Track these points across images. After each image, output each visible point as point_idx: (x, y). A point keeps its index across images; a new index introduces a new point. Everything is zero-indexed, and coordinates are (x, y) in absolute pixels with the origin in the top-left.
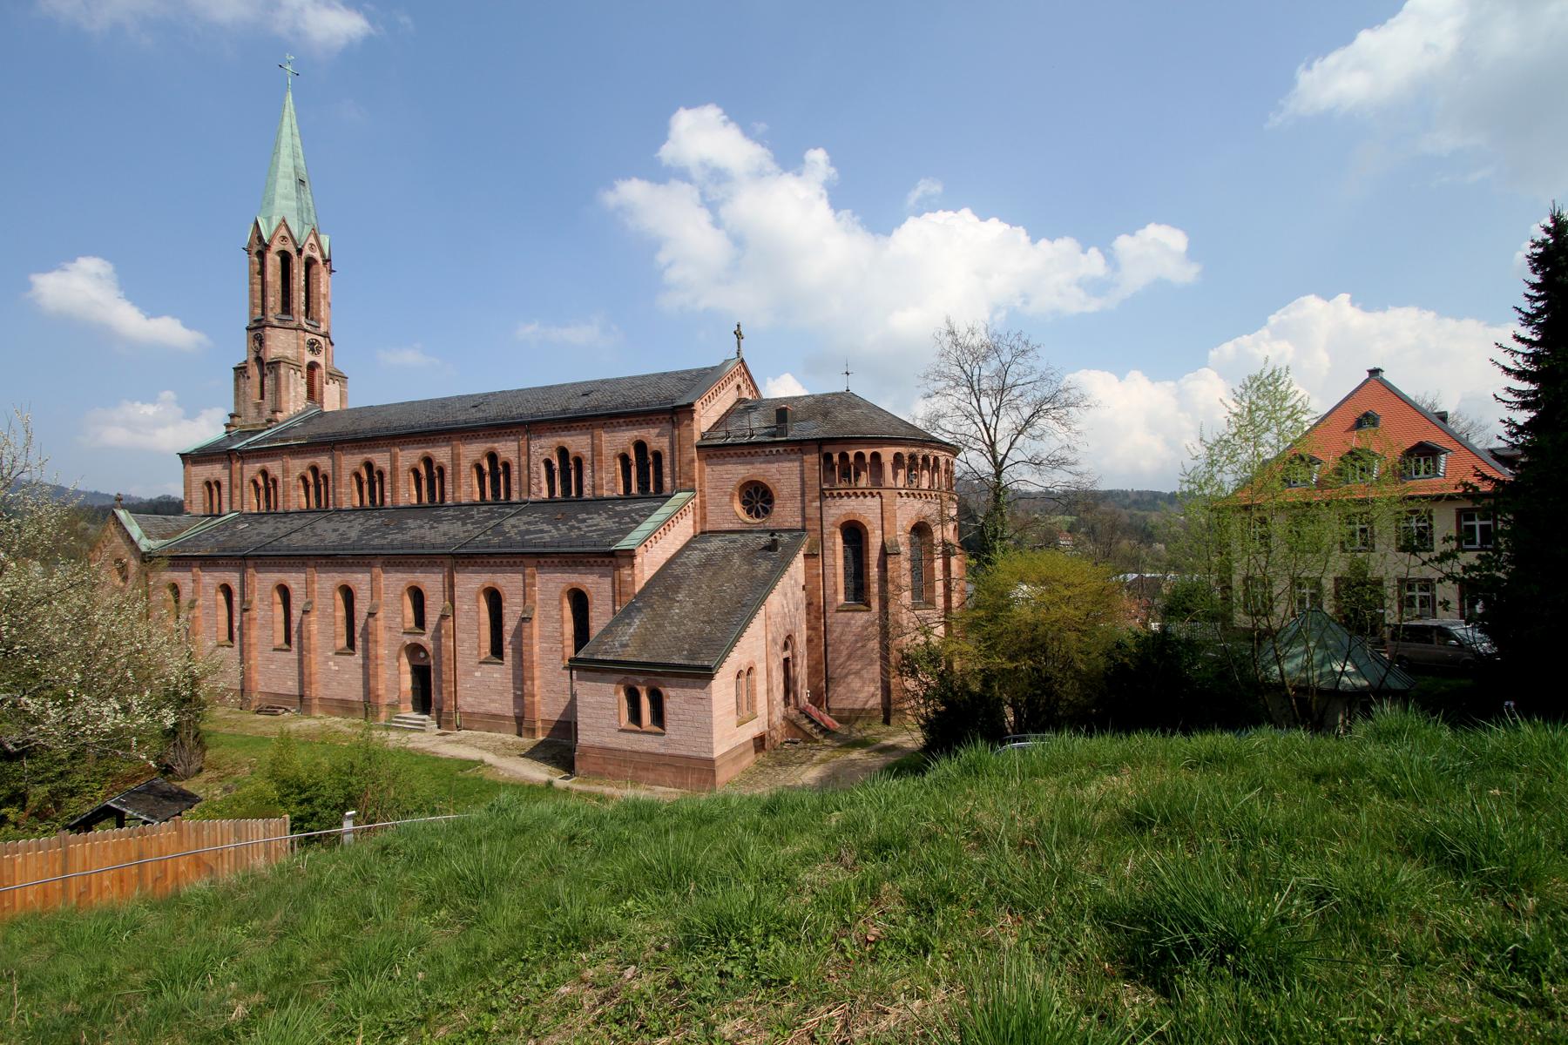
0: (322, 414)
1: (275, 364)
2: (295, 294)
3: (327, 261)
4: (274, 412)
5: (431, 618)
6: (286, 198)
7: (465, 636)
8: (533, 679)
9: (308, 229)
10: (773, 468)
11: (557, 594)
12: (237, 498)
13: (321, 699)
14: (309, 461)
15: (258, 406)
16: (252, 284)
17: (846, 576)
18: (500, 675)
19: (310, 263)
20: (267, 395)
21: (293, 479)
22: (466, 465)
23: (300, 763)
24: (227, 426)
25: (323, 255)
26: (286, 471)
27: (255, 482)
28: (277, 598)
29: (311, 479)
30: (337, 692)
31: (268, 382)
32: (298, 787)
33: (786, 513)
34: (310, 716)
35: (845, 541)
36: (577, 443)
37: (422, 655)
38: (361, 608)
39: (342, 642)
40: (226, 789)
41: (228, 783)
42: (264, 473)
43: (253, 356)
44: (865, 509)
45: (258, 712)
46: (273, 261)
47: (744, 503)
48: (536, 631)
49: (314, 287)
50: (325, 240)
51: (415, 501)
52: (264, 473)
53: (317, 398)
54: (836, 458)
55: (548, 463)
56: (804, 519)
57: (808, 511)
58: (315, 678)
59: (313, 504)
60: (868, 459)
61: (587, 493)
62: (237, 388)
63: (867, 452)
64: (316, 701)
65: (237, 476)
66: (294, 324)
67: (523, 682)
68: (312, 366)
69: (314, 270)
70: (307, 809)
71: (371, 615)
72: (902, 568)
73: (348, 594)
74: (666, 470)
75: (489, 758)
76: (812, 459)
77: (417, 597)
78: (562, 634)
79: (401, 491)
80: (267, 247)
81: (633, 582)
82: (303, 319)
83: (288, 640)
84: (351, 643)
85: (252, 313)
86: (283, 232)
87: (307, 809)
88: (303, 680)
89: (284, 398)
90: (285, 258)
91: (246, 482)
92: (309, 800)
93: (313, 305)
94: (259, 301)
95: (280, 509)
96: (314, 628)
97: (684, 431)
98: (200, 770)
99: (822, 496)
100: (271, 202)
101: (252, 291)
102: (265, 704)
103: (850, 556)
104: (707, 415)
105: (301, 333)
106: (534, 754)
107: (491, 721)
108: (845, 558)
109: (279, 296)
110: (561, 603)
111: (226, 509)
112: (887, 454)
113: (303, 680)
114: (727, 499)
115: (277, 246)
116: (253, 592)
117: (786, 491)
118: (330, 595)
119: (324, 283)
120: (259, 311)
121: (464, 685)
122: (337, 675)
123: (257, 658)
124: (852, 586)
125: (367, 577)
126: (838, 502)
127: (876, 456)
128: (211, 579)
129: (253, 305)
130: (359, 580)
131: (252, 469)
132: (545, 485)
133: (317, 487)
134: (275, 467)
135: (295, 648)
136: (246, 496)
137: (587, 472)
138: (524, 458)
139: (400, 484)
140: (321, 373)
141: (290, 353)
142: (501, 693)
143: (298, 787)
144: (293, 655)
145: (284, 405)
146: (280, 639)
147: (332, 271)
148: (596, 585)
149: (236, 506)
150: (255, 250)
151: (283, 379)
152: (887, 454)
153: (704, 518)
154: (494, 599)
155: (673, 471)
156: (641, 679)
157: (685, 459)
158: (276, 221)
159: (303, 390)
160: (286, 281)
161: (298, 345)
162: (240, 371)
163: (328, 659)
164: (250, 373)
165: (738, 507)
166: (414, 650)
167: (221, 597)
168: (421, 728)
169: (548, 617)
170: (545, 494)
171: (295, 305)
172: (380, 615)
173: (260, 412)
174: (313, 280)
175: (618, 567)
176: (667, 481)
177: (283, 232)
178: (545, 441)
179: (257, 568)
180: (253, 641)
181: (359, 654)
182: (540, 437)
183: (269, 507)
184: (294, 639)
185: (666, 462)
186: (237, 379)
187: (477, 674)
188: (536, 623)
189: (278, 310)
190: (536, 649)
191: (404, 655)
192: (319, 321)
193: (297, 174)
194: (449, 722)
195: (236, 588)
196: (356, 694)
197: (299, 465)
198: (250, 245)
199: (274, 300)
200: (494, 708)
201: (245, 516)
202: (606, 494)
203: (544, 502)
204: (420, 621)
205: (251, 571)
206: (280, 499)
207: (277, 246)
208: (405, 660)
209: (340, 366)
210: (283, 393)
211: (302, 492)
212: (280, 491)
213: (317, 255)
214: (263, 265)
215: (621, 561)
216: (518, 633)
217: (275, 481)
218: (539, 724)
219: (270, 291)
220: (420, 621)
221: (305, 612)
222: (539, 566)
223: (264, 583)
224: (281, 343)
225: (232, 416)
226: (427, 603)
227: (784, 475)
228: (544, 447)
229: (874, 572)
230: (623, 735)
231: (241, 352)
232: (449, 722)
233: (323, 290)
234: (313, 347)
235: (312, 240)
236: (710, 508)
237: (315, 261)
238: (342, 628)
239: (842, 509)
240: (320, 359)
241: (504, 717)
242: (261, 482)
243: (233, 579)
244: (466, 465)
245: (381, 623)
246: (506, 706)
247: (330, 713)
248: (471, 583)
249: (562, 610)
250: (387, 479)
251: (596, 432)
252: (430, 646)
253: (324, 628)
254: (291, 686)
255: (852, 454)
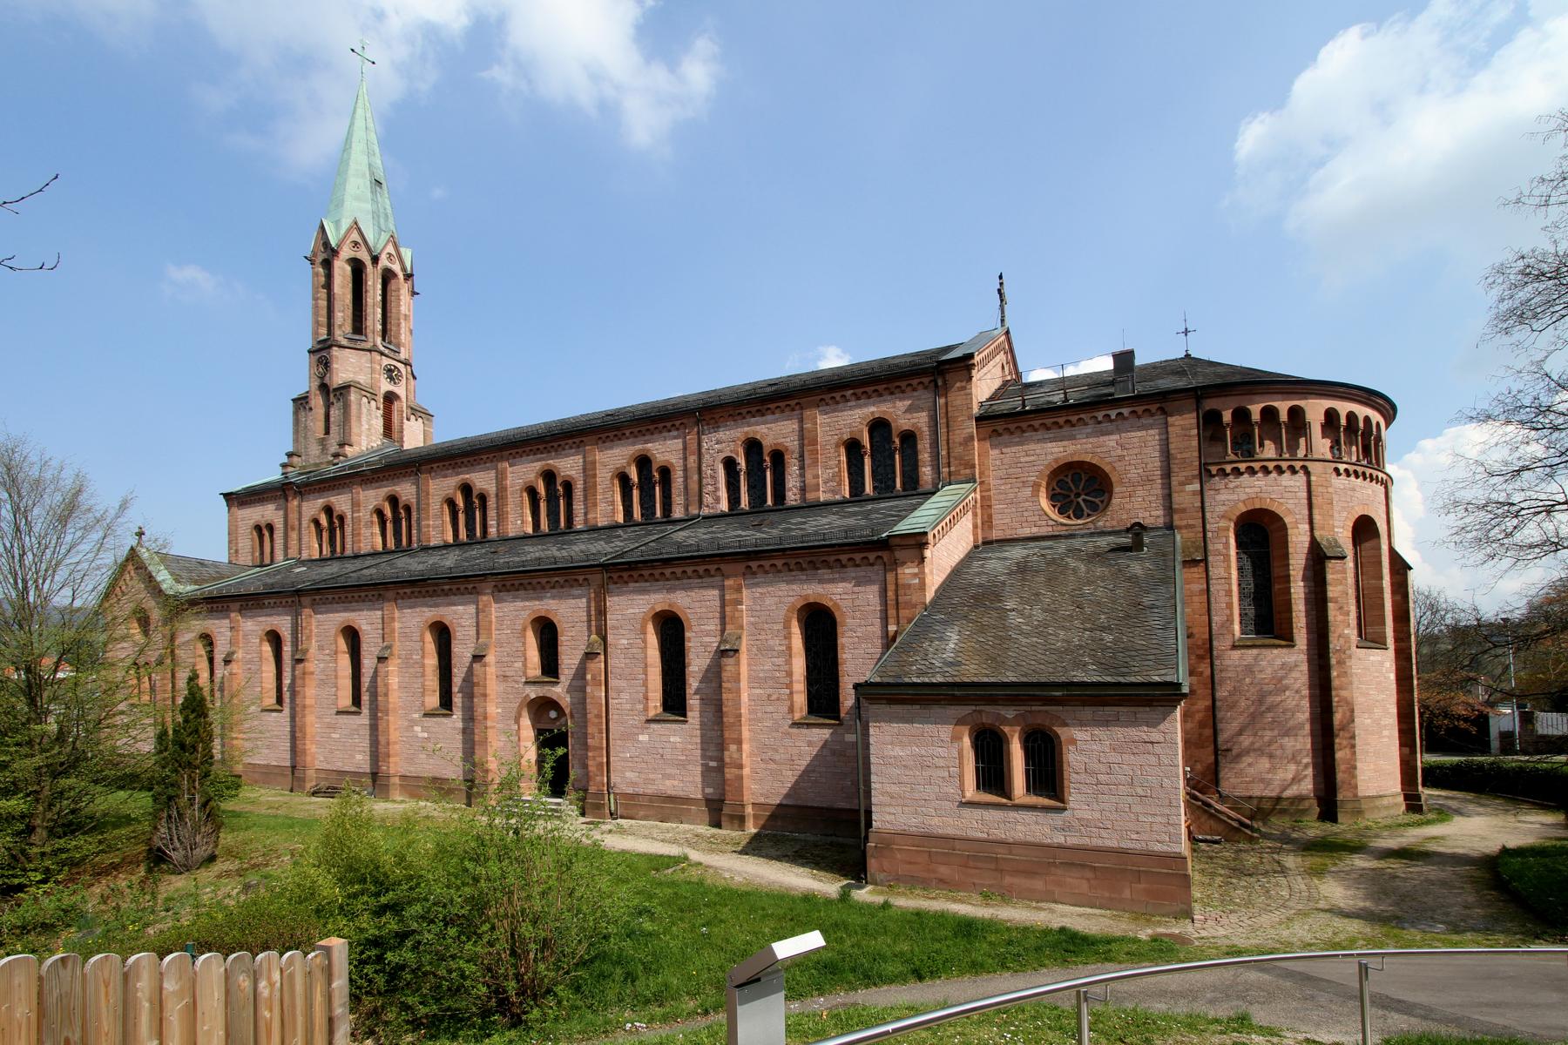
1: (345, 388)
2: (369, 310)
3: (409, 277)
4: (342, 445)
5: (569, 660)
6: (357, 198)
7: (623, 683)
8: (739, 742)
9: (384, 237)
10: (1111, 441)
11: (781, 613)
12: (293, 543)
13: (403, 777)
14: (384, 491)
15: (322, 442)
16: (316, 299)
17: (1242, 596)
18: (683, 737)
19: (388, 276)
20: (333, 428)
21: (366, 514)
22: (604, 476)
23: (384, 847)
24: (284, 466)
25: (404, 269)
26: (356, 505)
27: (316, 522)
28: (342, 645)
29: (388, 512)
30: (427, 766)
31: (335, 413)
32: (376, 882)
33: (1136, 502)
34: (387, 799)
35: (1239, 545)
36: (776, 431)
37: (553, 714)
38: (462, 652)
39: (433, 700)
40: (247, 888)
41: (253, 878)
42: (328, 510)
43: (317, 383)
44: (1281, 493)
45: (314, 794)
46: (342, 271)
47: (1053, 498)
48: (744, 669)
49: (392, 305)
50: (407, 254)
51: (530, 530)
52: (328, 510)
53: (396, 436)
54: (1227, 417)
55: (730, 464)
56: (1169, 509)
57: (1176, 498)
58: (394, 749)
59: (391, 544)
60: (1284, 417)
61: (792, 497)
62: (297, 422)
63: (1283, 406)
64: (396, 780)
65: (293, 517)
66: (369, 345)
67: (722, 747)
68: (390, 398)
69: (393, 285)
70: (391, 924)
71: (478, 658)
72: (1342, 581)
73: (442, 634)
74: (925, 457)
75: (694, 856)
76: (1184, 425)
77: (547, 633)
78: (790, 674)
79: (511, 517)
80: (335, 252)
81: (922, 586)
82: (379, 340)
83: (357, 700)
84: (446, 702)
85: (316, 333)
86: (355, 236)
87: (391, 924)
88: (377, 752)
89: (355, 430)
90: (357, 268)
91: (305, 523)
92: (395, 908)
93: (392, 321)
94: (323, 320)
95: (348, 552)
96: (394, 681)
97: (955, 398)
98: (212, 859)
99: (1204, 474)
100: (340, 204)
101: (316, 307)
102: (324, 784)
103: (1248, 566)
104: (985, 384)
105: (377, 356)
106: (755, 847)
107: (667, 807)
108: (1240, 569)
109: (349, 312)
110: (787, 626)
111: (279, 555)
112: (1315, 410)
113: (377, 752)
114: (1028, 492)
115: (346, 252)
116: (309, 638)
117: (1133, 474)
118: (416, 637)
119: (404, 303)
120: (323, 331)
121: (622, 754)
122: (422, 742)
123: (313, 723)
124: (1251, 612)
125: (472, 609)
126: (1233, 482)
127: (1296, 413)
128: (253, 627)
129: (317, 323)
130: (459, 615)
131: (312, 507)
132: (723, 494)
133: (397, 521)
134: (341, 502)
135: (365, 710)
136: (305, 539)
137: (792, 470)
138: (692, 459)
139: (510, 508)
141: (363, 379)
142: (682, 765)
143: (376, 882)
144: (364, 719)
145: (354, 439)
146: (346, 700)
147: (414, 293)
148: (855, 601)
149: (293, 552)
150: (320, 259)
151: (354, 408)
152: (1315, 410)
153: (988, 522)
154: (671, 629)
155: (936, 456)
156: (1010, 713)
157: (958, 437)
158: (345, 224)
159: (378, 424)
160: (357, 294)
161: (373, 371)
162: (301, 403)
163: (413, 723)
164: (312, 403)
165: (1044, 503)
166: (541, 708)
167: (267, 649)
168: (555, 814)
169: (763, 650)
170: (724, 506)
171: (369, 323)
172: (490, 659)
173: (324, 449)
174: (392, 298)
175: (895, 564)
176: (926, 472)
177: (355, 236)
178: (723, 434)
179: (316, 607)
180: (308, 702)
181: (457, 715)
182: (716, 428)
183: (333, 551)
184: (365, 698)
185: (924, 446)
186: (296, 413)
187: (643, 738)
188: (744, 658)
189: (348, 328)
190: (745, 697)
191: (525, 714)
192: (398, 346)
193: (372, 174)
194: (598, 807)
195: (286, 634)
196: (453, 770)
197: (372, 497)
198: (314, 253)
199: (343, 315)
200: (671, 786)
201: (301, 563)
202: (823, 497)
203: (723, 515)
204: (550, 666)
205: (307, 611)
206: (349, 540)
207: (346, 252)
208: (526, 722)
209: (423, 402)
210: (354, 423)
211: (377, 530)
212: (348, 530)
213: (396, 268)
214: (329, 277)
215: (899, 554)
216: (714, 674)
217: (341, 518)
218: (749, 810)
219: (338, 305)
220: (550, 666)
221: (381, 659)
222: (749, 573)
223: (323, 626)
224: (349, 366)
225: (290, 455)
226: (562, 639)
227: (1130, 452)
228: (724, 442)
229: (1298, 590)
230: (967, 812)
231: (302, 379)
232: (598, 807)
233: (403, 309)
234: (391, 374)
235: (390, 249)
236: (997, 507)
237: (395, 275)
238: (433, 681)
239: (1237, 494)
240: (400, 390)
242: (324, 521)
243: (283, 623)
244: (604, 476)
245: (492, 671)
246: (689, 783)
247: (416, 796)
248: (631, 610)
249: (788, 637)
250: (492, 503)
251: (807, 413)
252: (566, 701)
253: (407, 680)
254: (360, 760)
255: (1255, 410)
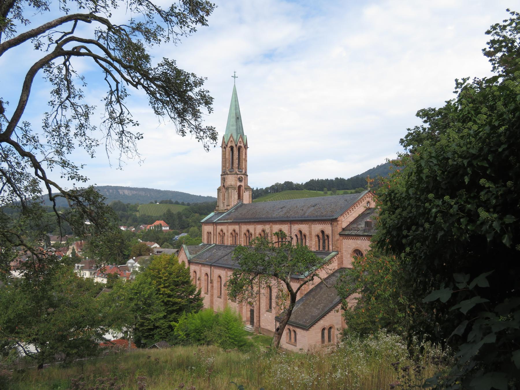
0: (243, 204)
25: (244, 144)
66: (234, 172)
68: (240, 187)
89: (230, 201)
111: (212, 243)
115: (229, 145)
140: (243, 188)
151: (230, 194)
159: (236, 196)
177: (231, 139)
213: (242, 145)
234: (240, 180)
235: (240, 140)
240: (242, 184)
241: (271, 331)
